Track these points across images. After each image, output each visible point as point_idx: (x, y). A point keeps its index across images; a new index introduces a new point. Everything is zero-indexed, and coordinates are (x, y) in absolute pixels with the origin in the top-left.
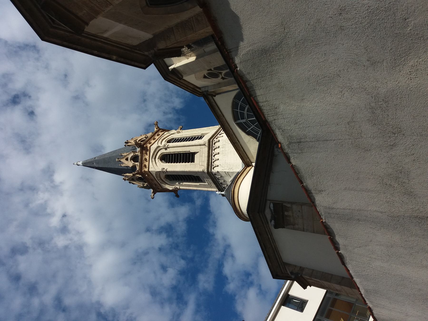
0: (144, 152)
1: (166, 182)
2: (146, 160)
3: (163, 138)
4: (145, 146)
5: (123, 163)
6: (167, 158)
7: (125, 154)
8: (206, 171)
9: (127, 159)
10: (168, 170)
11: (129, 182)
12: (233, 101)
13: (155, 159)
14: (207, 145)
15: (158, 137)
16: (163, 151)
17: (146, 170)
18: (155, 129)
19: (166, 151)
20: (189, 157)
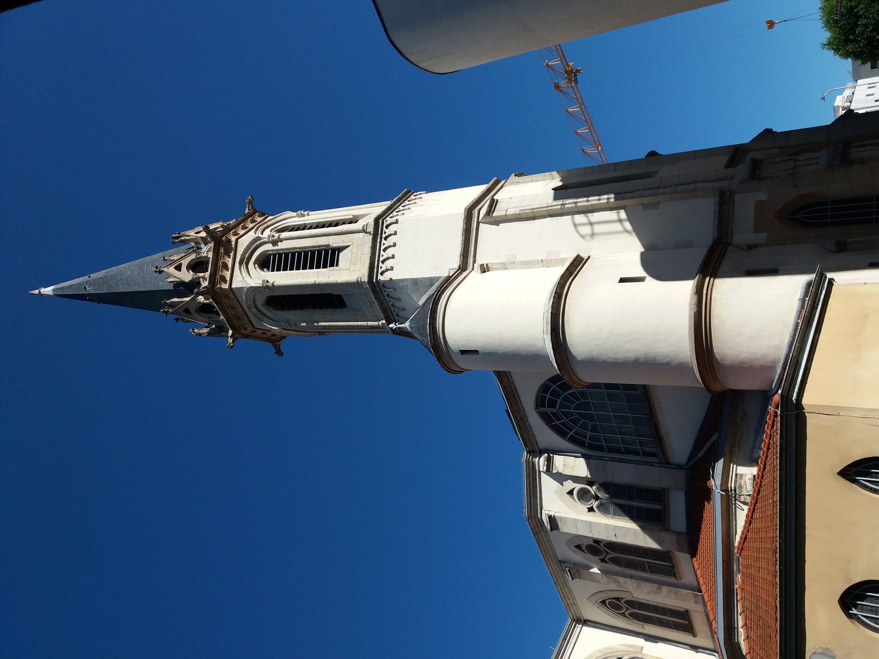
2: (225, 266)
3: (265, 225)
4: (224, 238)
5: (170, 276)
8: (365, 279)
9: (178, 268)
11: (177, 320)
13: (247, 264)
14: (371, 229)
15: (251, 226)
16: (269, 247)
17: (225, 286)
18: (247, 211)
19: (276, 248)
20: (327, 257)
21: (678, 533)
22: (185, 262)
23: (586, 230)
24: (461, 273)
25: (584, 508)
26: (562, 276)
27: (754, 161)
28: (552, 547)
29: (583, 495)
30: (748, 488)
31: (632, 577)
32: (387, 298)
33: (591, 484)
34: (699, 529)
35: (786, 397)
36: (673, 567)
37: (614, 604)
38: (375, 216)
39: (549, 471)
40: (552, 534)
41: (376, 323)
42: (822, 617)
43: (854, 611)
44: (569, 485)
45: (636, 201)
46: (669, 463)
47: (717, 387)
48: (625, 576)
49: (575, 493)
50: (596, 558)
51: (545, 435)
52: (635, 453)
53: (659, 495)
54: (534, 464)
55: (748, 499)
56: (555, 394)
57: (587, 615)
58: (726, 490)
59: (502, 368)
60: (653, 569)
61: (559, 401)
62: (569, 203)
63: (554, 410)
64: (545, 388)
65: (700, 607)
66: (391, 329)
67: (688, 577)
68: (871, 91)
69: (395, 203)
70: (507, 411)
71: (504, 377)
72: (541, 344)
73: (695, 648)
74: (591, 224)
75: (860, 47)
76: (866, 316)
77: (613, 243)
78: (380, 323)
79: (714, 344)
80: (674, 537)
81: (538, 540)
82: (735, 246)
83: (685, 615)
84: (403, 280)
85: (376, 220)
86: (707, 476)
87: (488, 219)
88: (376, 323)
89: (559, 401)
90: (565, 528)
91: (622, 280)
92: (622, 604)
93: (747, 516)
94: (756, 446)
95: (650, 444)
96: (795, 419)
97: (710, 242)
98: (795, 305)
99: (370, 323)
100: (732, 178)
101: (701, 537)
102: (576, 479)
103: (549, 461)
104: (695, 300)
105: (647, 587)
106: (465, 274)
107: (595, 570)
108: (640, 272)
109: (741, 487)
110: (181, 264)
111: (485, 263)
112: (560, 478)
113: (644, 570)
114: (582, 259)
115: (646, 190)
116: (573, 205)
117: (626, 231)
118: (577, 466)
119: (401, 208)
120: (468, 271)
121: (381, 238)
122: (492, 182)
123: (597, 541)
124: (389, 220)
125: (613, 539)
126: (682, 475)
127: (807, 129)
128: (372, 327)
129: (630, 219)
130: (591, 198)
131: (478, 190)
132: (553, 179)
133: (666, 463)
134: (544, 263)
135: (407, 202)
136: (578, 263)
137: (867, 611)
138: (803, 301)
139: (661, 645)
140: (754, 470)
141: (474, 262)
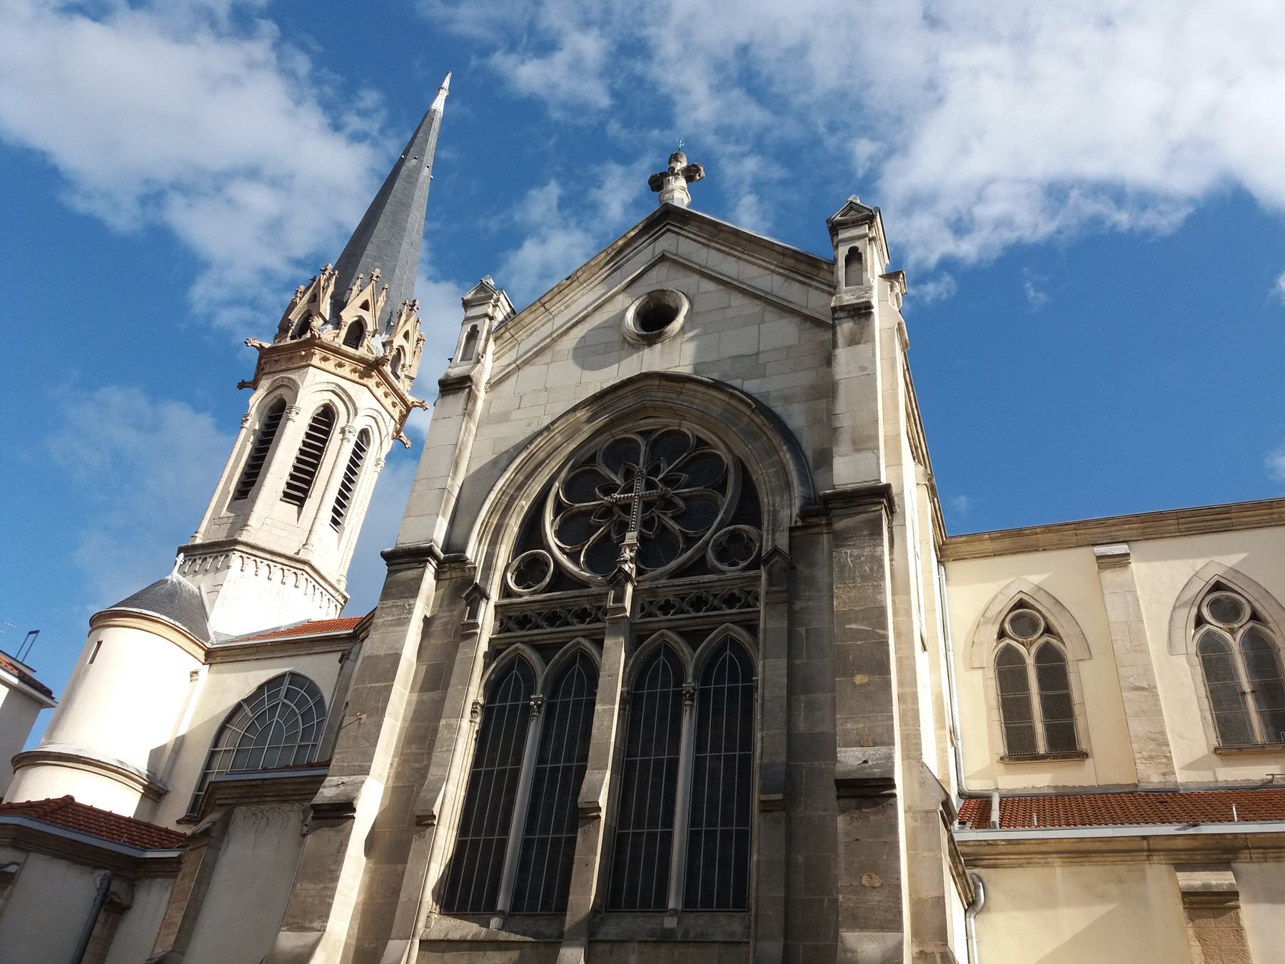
0: (360, 367)
1: (271, 396)
2: (340, 365)
6: (325, 418)
7: (381, 303)
8: (244, 537)
10: (290, 423)
12: (319, 692)
13: (333, 392)
17: (316, 360)
20: (298, 491)
22: (368, 316)
38: (645, 369)
56: (306, 716)
110: (367, 309)
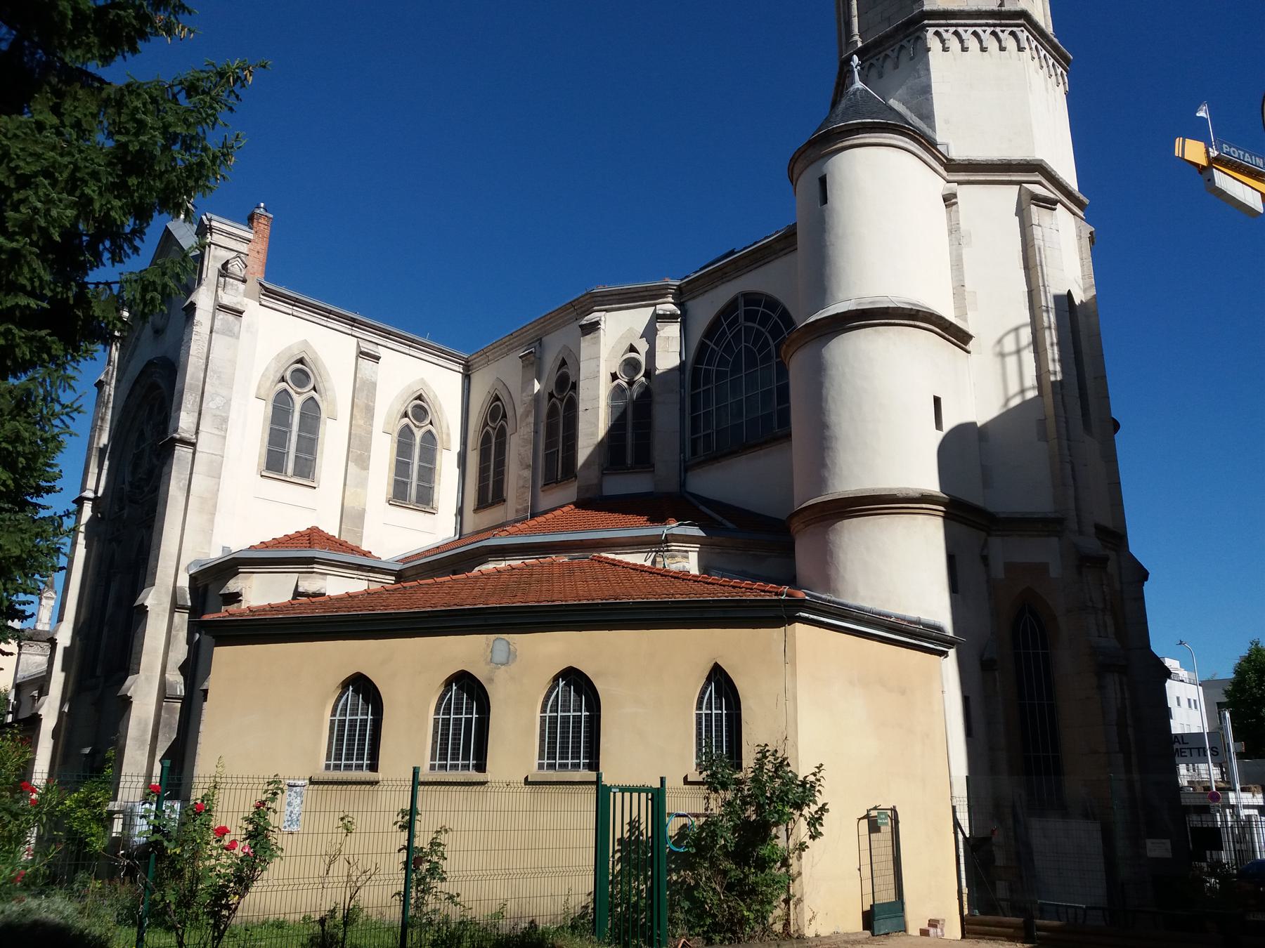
8: (927, 7)
21: (600, 485)
23: (1009, 345)
24: (942, 164)
25: (615, 368)
26: (941, 318)
27: (1105, 560)
28: (558, 327)
29: (631, 366)
30: (675, 565)
31: (536, 432)
32: (897, 46)
33: (648, 374)
34: (611, 510)
35: (802, 605)
36: (557, 482)
37: (496, 412)
39: (657, 318)
40: (574, 328)
41: (856, 30)
42: (555, 649)
43: (561, 684)
44: (643, 346)
45: (1050, 411)
46: (686, 471)
47: (796, 525)
48: (536, 424)
49: (633, 355)
50: (553, 387)
51: (706, 308)
52: (695, 429)
53: (644, 460)
54: (664, 296)
55: (659, 566)
56: (765, 320)
57: (476, 378)
58: (666, 541)
59: (803, 235)
60: (550, 458)
61: (756, 326)
62: (1049, 319)
63: (741, 319)
64: (772, 304)
65: (511, 516)
66: (850, 59)
67: (546, 501)
68: (1184, 703)
69: (1049, 41)
70: (732, 253)
71: (787, 241)
72: (841, 296)
73: (460, 512)
74: (1018, 352)
75: (1251, 688)
76: (903, 692)
77: (988, 383)
78: (857, 38)
79: (885, 519)
80: (595, 481)
81: (563, 309)
82: (986, 540)
83: (499, 499)
84: (928, 70)
85: (1024, 15)
86: (681, 518)
87: (1025, 198)
88: (856, 30)
89: (756, 326)
90: (586, 342)
91: (937, 401)
92: (499, 423)
93: (642, 566)
94: (723, 572)
95: (709, 447)
96: (778, 615)
97: (991, 509)
98: (913, 614)
99: (855, 20)
100: (1081, 532)
101: (602, 514)
102: (651, 355)
103: (670, 318)
104: (912, 494)
105: (528, 452)
106: (941, 169)
107: (537, 386)
108: (949, 423)
109: (673, 557)
111: (959, 200)
112: (650, 334)
113: (547, 447)
114: (966, 343)
115: (1067, 422)
116: (1046, 324)
117: (1008, 400)
118: (668, 357)
119: (1043, 52)
120: (945, 173)
121: (995, 25)
122: (1082, 197)
123: (575, 386)
124: (1023, 35)
125: (581, 407)
126: (673, 487)
127: (1146, 623)
128: (848, 24)
129: (1025, 404)
130: (1056, 348)
131: (1068, 173)
132: (1085, 291)
133: (686, 468)
134: (959, 289)
135: (1051, 61)
136: (960, 337)
137: (564, 696)
138: (918, 622)
139: (456, 472)
140: (694, 570)
141: (960, 183)
